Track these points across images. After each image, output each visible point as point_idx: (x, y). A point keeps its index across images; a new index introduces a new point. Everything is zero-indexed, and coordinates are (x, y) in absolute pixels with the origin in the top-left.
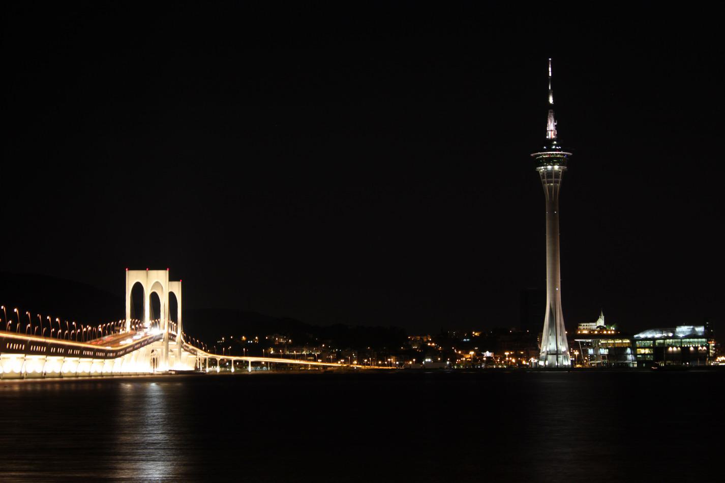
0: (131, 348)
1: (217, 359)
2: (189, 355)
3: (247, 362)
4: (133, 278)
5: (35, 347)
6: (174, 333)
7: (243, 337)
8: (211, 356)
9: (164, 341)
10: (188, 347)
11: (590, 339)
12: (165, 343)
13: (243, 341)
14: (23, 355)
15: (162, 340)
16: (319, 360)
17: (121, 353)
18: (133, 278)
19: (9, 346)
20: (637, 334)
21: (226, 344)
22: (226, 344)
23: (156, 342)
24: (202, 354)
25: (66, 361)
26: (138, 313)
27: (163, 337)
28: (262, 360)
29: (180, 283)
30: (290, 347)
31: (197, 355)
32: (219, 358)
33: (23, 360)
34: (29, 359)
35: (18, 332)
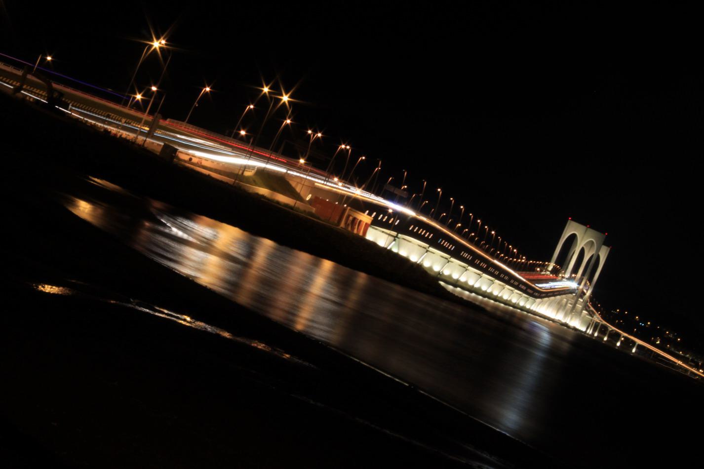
0: (549, 294)
1: (609, 328)
2: (587, 315)
3: (634, 343)
4: (572, 228)
5: (451, 246)
6: (585, 291)
7: (657, 343)
8: (604, 323)
9: (575, 296)
10: (589, 307)
11: (252, 347)
12: (575, 298)
13: (636, 320)
14: (426, 245)
15: (574, 294)
16: (701, 371)
17: (544, 295)
18: (572, 228)
19: (429, 235)
20: (187, 326)
21: (621, 316)
22: (621, 316)
23: (570, 295)
24: (598, 318)
25: (468, 270)
26: (562, 261)
27: (577, 291)
28: (578, 275)
29: (609, 249)
30: (678, 346)
31: (593, 317)
32: (612, 328)
33: (447, 261)
34: (452, 262)
35: (455, 231)
